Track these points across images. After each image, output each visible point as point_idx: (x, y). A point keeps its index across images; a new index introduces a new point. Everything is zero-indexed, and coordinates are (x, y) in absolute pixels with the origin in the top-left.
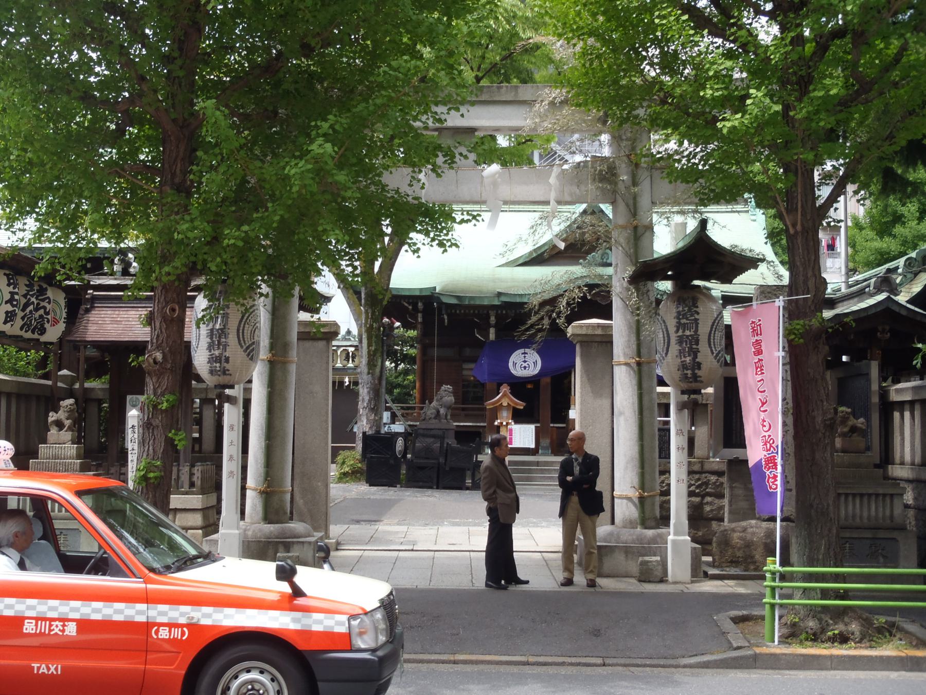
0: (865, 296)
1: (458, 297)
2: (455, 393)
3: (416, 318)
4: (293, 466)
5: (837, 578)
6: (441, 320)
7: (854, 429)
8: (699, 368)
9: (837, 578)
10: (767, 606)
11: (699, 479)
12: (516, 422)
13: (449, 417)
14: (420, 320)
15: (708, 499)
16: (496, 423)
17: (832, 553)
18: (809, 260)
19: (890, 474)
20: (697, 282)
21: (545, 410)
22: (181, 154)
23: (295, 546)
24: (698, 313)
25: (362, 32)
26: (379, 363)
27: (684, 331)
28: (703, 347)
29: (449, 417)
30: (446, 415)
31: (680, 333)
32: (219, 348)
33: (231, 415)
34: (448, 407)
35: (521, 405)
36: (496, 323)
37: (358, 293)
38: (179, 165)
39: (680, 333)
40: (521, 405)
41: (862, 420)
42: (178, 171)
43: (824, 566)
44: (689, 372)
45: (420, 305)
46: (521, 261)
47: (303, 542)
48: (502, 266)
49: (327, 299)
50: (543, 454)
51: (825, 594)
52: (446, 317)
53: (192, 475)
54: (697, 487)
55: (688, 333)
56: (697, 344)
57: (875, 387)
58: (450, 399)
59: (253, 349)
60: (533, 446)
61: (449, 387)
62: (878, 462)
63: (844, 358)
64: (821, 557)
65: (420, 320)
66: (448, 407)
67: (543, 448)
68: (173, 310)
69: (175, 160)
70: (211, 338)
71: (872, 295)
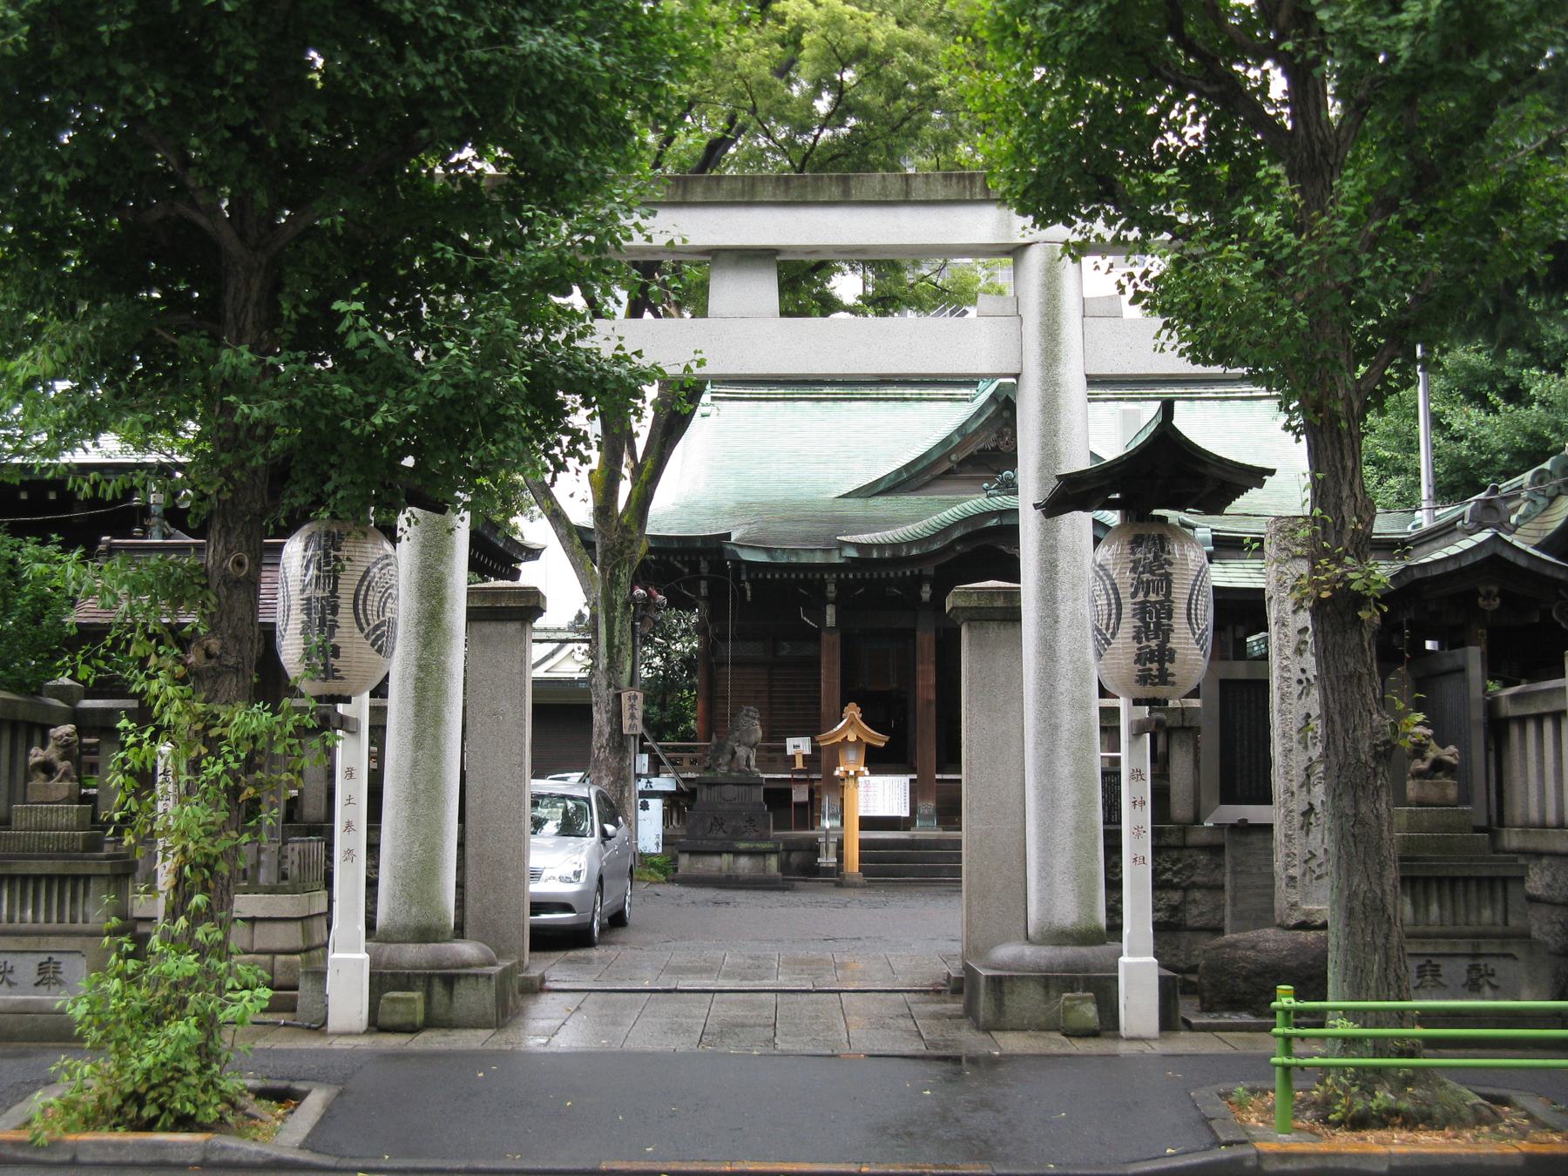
0: (1457, 535)
3: (697, 591)
4: (461, 845)
5: (1401, 1018)
7: (1438, 765)
8: (1172, 660)
9: (1401, 1018)
10: (1278, 1070)
11: (1179, 860)
12: (873, 772)
14: (703, 592)
15: (1197, 895)
16: (837, 773)
17: (1391, 977)
18: (1344, 468)
19: (1506, 843)
20: (1156, 512)
21: (927, 749)
22: (254, 295)
23: (462, 982)
24: (1171, 564)
25: (216, 92)
26: (628, 669)
27: (1146, 595)
28: (1179, 621)
31: (1140, 597)
32: (322, 631)
33: (351, 754)
35: (880, 740)
37: (589, 546)
38: (251, 314)
39: (1140, 597)
40: (880, 740)
41: (1452, 749)
42: (249, 326)
43: (1378, 1000)
44: (1155, 666)
45: (704, 567)
46: (881, 487)
47: (476, 976)
48: (844, 496)
49: (534, 554)
51: (1381, 1047)
52: (748, 586)
53: (283, 857)
54: (1175, 874)
55: (1153, 597)
56: (1170, 617)
57: (1476, 693)
59: (382, 635)
60: (905, 813)
62: (1483, 822)
63: (1429, 645)
64: (1373, 984)
65: (703, 592)
68: (240, 563)
69: (244, 306)
70: (309, 615)
71: (1470, 533)
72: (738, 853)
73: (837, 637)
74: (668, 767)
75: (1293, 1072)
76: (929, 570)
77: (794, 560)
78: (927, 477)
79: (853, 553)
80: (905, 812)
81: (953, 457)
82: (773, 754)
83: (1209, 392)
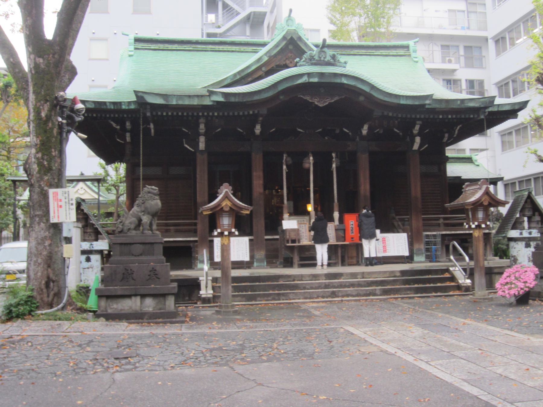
1: (165, 96)
2: (162, 195)
6: (147, 131)
13: (154, 227)
21: (259, 224)
29: (154, 227)
30: (151, 225)
34: (154, 215)
36: (206, 132)
45: (128, 125)
46: (226, 83)
50: (258, 267)
58: (156, 203)
61: (155, 189)
66: (154, 215)
67: (259, 261)
72: (143, 296)
73: (205, 156)
74: (104, 235)
75: (17, 183)
76: (264, 111)
77: (180, 103)
78: (250, 79)
79: (221, 99)
80: (247, 258)
81: (263, 69)
82: (168, 228)
83: (378, 52)
